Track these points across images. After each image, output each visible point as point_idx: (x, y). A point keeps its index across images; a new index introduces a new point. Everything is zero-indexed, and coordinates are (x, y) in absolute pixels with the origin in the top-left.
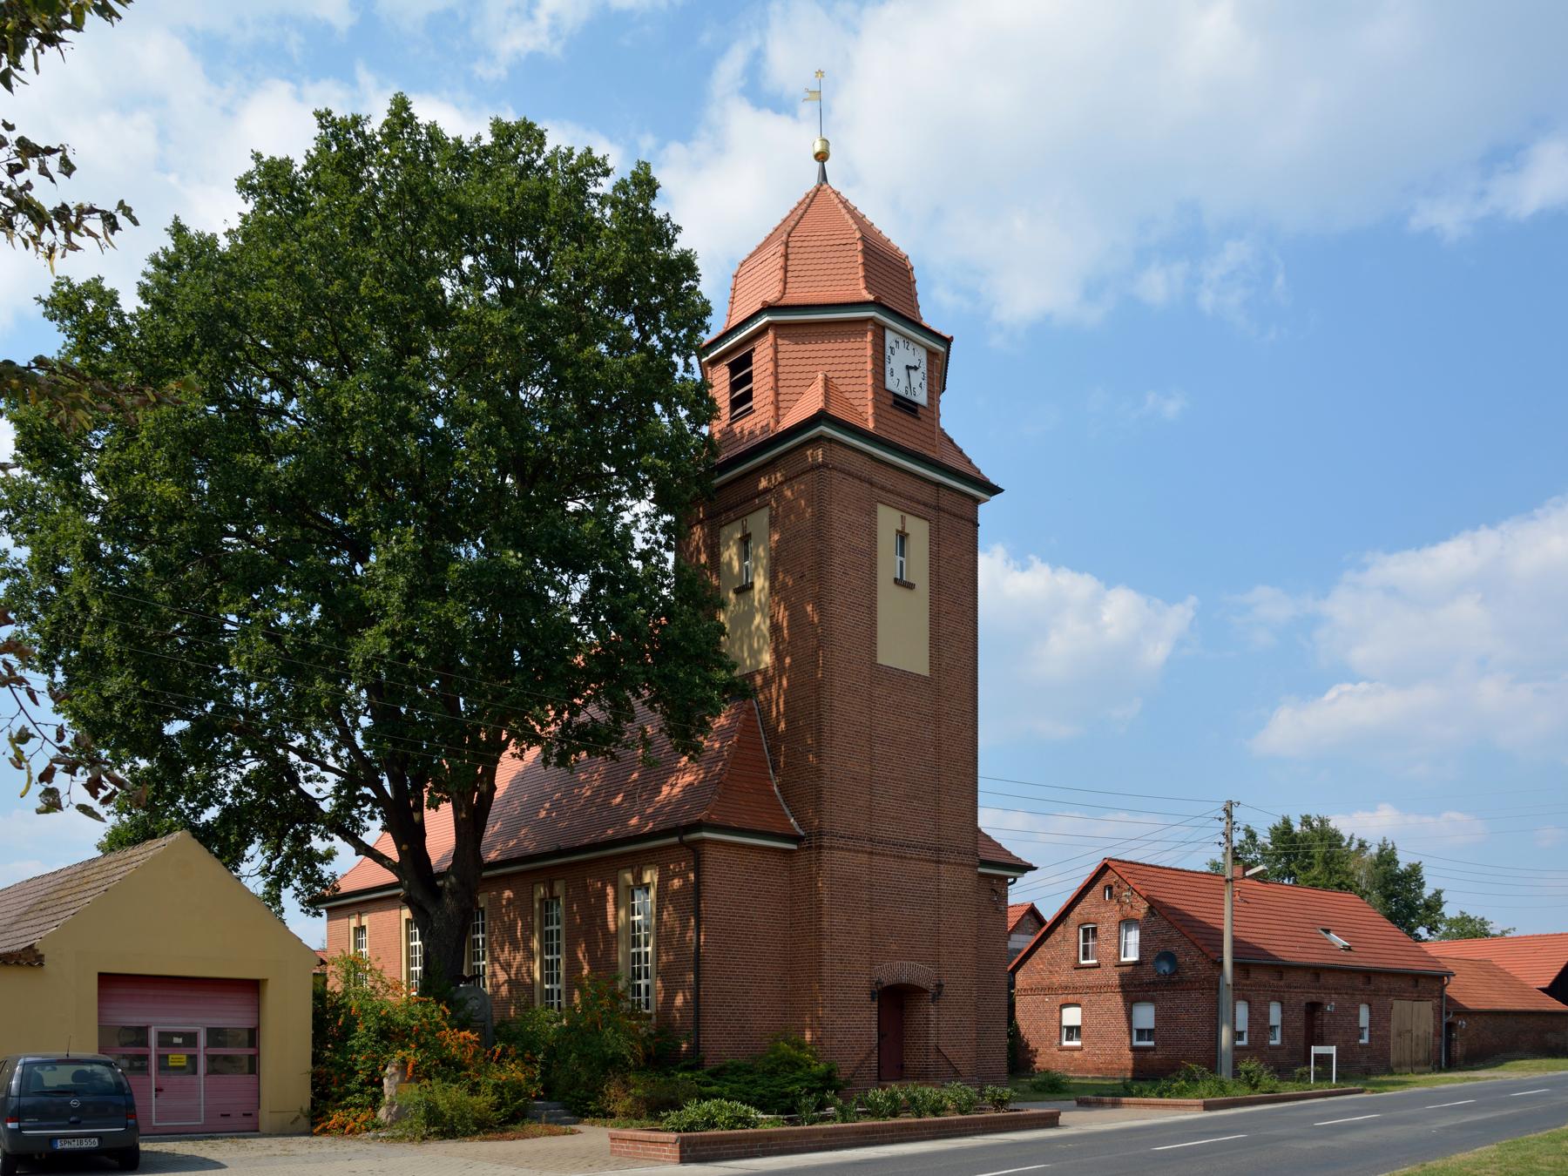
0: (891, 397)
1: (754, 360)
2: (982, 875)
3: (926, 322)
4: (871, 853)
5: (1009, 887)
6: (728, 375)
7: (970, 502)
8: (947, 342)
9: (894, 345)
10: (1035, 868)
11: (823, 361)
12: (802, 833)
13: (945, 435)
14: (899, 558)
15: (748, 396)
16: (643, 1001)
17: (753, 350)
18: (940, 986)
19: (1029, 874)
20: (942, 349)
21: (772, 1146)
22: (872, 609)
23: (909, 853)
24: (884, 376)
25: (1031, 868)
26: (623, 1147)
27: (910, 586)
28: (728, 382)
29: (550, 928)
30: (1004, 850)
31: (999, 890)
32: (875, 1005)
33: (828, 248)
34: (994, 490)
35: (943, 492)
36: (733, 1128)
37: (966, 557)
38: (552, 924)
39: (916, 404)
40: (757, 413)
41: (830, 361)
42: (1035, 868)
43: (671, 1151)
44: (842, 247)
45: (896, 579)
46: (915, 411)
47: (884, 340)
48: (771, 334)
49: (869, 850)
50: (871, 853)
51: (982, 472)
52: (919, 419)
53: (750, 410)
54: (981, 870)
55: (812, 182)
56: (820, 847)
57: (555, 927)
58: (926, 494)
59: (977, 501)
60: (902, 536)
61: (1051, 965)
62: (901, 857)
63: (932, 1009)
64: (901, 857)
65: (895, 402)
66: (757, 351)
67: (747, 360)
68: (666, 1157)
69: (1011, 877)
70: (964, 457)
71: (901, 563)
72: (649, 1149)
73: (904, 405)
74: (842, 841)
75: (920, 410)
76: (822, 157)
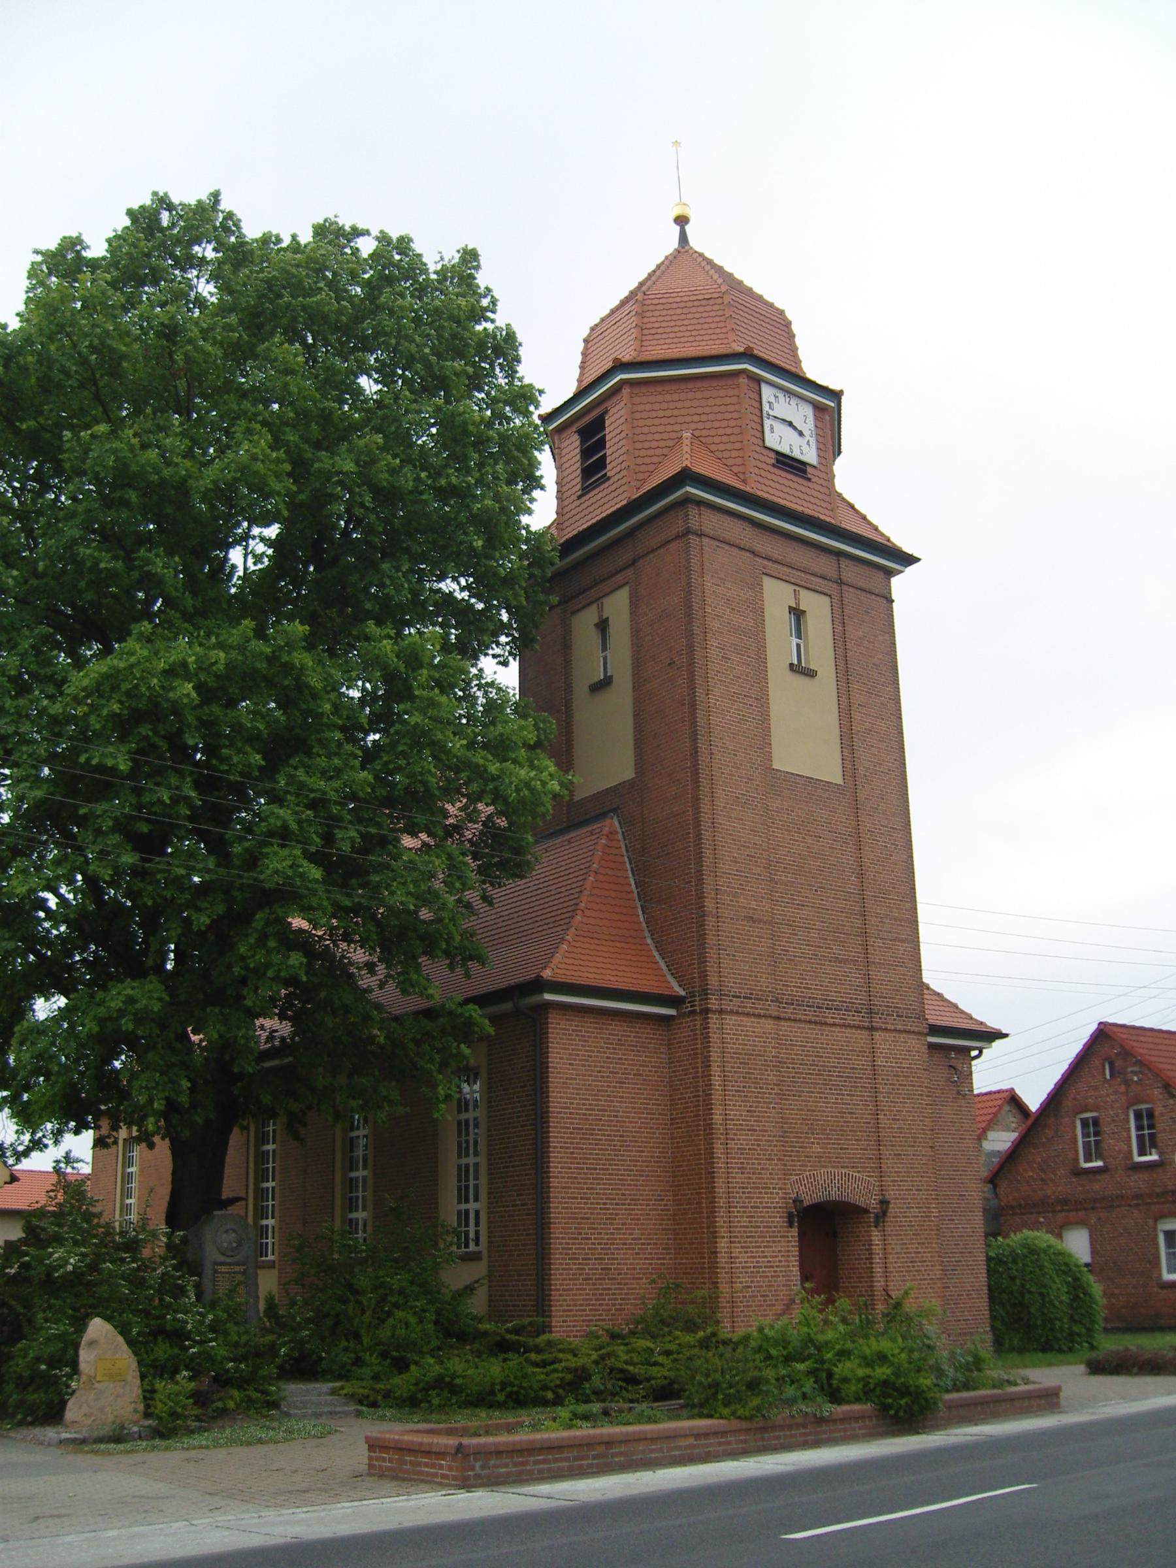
0: (773, 455)
1: (607, 423)
2: (932, 1047)
3: (811, 375)
4: (778, 1018)
5: (973, 1063)
6: (578, 443)
7: (881, 575)
8: (836, 395)
9: (772, 399)
10: (1006, 1035)
11: (689, 419)
12: (683, 993)
13: (844, 500)
14: (795, 641)
15: (601, 464)
16: (472, 1235)
17: (606, 412)
18: (884, 1203)
19: (997, 1043)
20: (832, 404)
21: (614, 1455)
22: (762, 701)
23: (829, 1017)
24: (763, 432)
25: (1001, 1035)
26: (384, 1459)
27: (811, 674)
28: (578, 450)
29: (464, 1161)
30: (962, 1012)
31: (959, 1067)
32: (794, 1232)
33: (691, 304)
34: (909, 560)
35: (844, 563)
36: (571, 1427)
37: (881, 638)
38: (467, 1155)
39: (804, 464)
40: (611, 481)
41: (696, 418)
42: (1006, 1035)
43: (450, 1468)
44: (704, 303)
45: (791, 665)
46: (804, 472)
47: (760, 395)
48: (626, 391)
49: (775, 1014)
50: (778, 1018)
51: (892, 539)
52: (809, 480)
53: (605, 478)
54: (931, 1039)
55: (673, 244)
56: (706, 1011)
57: (471, 1160)
58: (825, 565)
59: (890, 573)
60: (797, 614)
61: (1043, 1171)
62: (821, 1023)
63: (876, 1236)
64: (821, 1023)
65: (778, 461)
66: (611, 413)
67: (598, 425)
68: (444, 1476)
69: (975, 1048)
70: (870, 523)
71: (798, 646)
72: (419, 1464)
73: (788, 464)
74: (737, 1002)
75: (809, 469)
76: (682, 221)
